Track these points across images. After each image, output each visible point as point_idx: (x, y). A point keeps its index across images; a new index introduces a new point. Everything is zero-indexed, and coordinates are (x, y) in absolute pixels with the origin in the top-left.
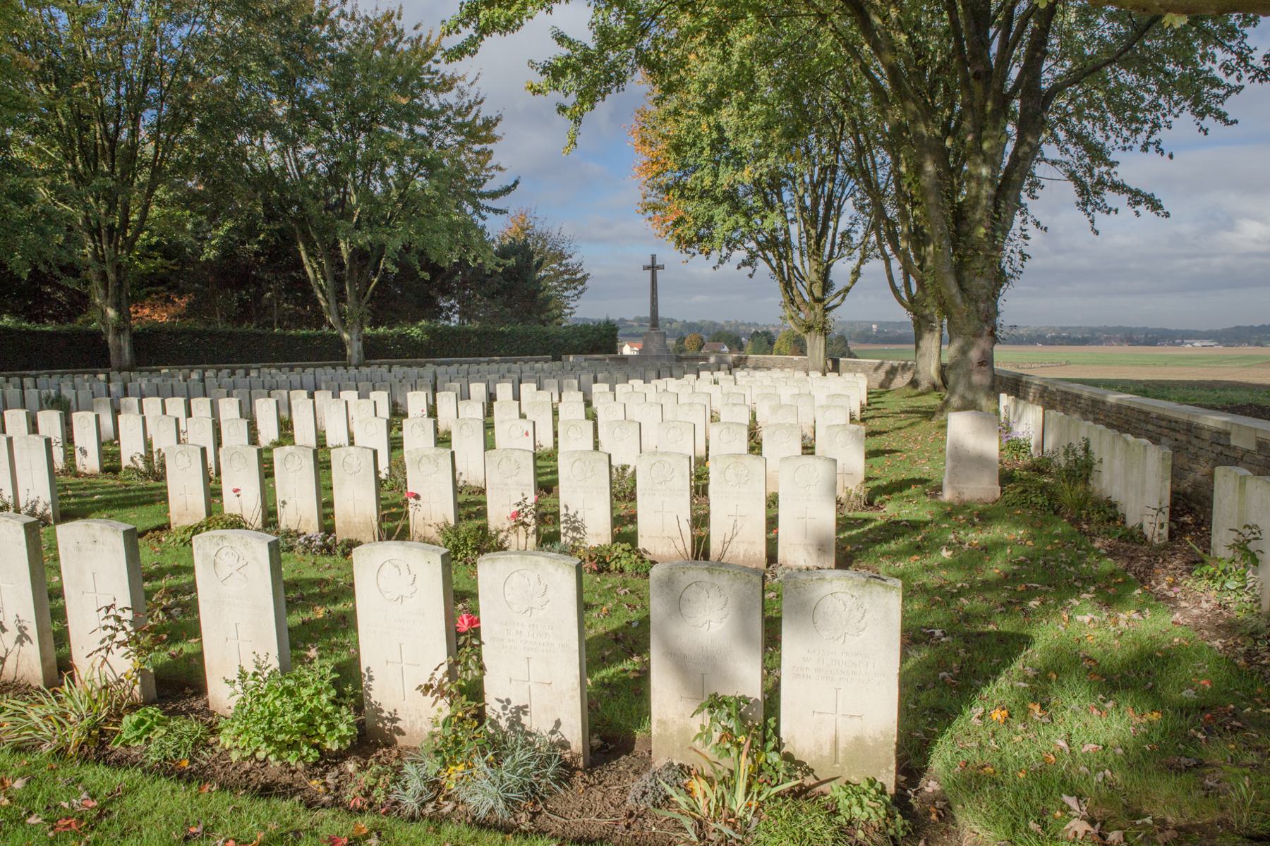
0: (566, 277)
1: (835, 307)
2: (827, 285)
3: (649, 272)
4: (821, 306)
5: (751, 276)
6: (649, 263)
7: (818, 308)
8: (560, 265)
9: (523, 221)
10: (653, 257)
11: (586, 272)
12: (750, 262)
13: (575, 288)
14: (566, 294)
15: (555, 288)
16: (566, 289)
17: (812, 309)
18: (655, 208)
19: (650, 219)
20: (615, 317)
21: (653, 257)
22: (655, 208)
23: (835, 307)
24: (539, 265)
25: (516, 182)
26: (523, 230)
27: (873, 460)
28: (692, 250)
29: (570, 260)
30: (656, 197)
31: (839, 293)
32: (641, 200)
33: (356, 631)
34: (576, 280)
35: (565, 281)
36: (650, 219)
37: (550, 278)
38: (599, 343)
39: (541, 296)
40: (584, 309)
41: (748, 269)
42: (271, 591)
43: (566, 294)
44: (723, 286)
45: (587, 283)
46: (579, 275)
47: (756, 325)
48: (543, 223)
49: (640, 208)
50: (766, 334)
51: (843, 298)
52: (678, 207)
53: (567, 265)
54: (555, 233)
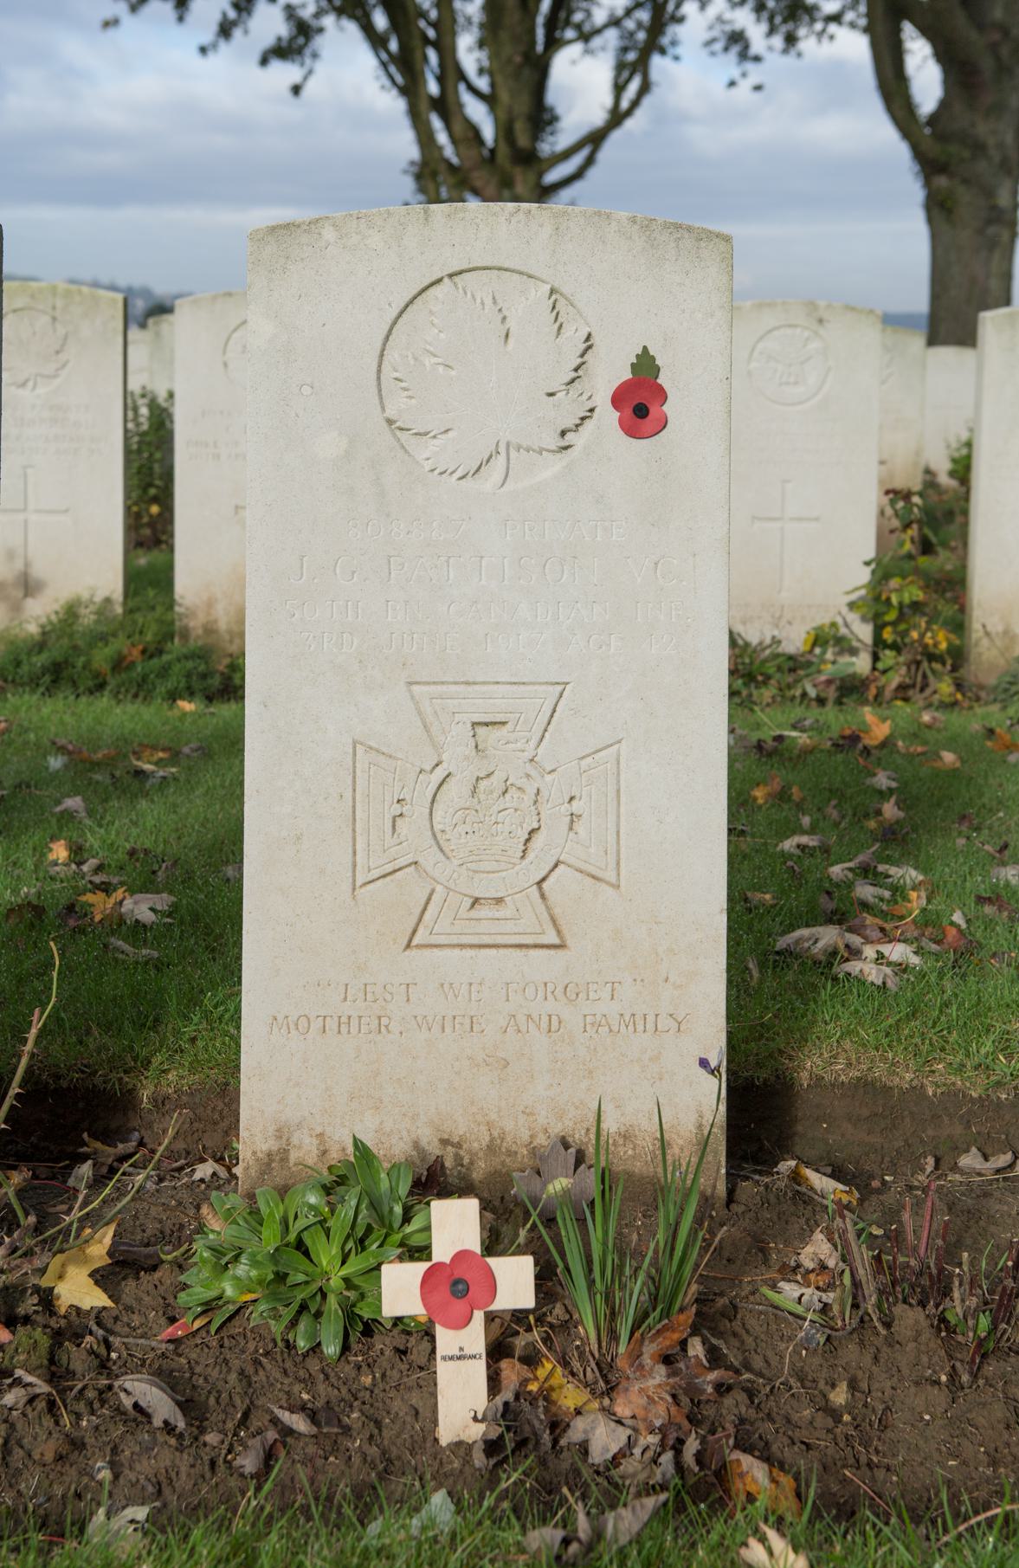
2: (541, 118)
4: (531, 177)
41: (285, 73)
51: (590, 161)
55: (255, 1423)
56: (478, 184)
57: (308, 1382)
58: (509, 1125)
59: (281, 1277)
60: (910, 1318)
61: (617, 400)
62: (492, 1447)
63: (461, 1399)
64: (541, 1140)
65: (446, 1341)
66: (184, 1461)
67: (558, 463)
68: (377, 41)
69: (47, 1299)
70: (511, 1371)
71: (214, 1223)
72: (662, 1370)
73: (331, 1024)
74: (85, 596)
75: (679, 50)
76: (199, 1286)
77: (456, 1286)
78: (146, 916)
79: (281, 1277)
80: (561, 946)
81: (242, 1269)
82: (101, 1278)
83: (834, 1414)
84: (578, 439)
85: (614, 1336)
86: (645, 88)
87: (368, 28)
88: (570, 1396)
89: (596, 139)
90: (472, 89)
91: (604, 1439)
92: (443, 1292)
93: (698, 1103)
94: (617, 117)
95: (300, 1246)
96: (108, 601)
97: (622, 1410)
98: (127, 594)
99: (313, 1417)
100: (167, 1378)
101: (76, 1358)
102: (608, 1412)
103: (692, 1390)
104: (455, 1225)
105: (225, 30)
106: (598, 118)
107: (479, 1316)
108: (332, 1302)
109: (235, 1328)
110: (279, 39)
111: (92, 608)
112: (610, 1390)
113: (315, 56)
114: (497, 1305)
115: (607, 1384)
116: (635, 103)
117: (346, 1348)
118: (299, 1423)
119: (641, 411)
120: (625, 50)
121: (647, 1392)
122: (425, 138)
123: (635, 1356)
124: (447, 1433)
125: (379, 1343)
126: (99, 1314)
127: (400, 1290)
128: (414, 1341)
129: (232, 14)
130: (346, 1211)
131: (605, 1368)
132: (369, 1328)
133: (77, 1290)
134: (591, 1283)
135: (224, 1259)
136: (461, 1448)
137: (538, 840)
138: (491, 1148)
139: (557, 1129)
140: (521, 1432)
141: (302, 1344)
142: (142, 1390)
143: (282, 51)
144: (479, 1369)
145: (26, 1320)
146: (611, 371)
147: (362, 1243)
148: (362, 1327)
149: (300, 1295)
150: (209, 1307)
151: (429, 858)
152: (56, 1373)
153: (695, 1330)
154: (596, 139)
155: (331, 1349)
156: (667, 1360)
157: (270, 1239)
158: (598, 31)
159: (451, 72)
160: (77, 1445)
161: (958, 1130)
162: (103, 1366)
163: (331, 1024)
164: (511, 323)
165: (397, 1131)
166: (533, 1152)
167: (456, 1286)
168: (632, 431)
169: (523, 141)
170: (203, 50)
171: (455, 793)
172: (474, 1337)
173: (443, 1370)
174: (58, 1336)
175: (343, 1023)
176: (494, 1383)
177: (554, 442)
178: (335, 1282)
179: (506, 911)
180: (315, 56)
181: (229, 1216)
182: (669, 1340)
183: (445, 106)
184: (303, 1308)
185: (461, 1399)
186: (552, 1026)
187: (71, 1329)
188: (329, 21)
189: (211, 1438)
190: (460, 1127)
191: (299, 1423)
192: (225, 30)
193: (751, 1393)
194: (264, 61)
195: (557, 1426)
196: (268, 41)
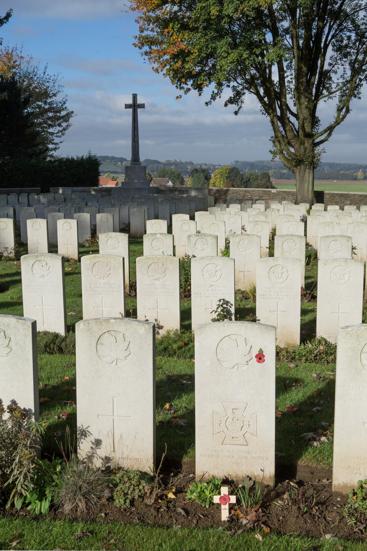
0: (51, 115)
1: (322, 142)
2: (315, 121)
3: (131, 110)
4: (310, 141)
5: (236, 113)
6: (130, 102)
7: (308, 143)
8: (45, 103)
9: (9, 60)
10: (135, 97)
11: (70, 110)
12: (236, 99)
13: (60, 125)
14: (51, 130)
15: (40, 124)
16: (50, 126)
17: (302, 143)
18: (151, 42)
19: (146, 53)
20: (98, 152)
21: (135, 97)
22: (151, 42)
23: (322, 142)
24: (27, 103)
25: (8, 16)
26: (10, 68)
27: (96, 249)
28: (185, 87)
29: (54, 99)
30: (152, 32)
31: (325, 131)
32: (138, 34)
33: (276, 418)
34: (61, 116)
35: (49, 118)
36: (146, 53)
37: (37, 116)
38: (82, 174)
39: (28, 131)
40: (67, 146)
41: (233, 107)
42: (31, 347)
43: (51, 130)
44: (224, 123)
45: (71, 120)
46: (63, 113)
47: (191, 163)
48: (28, 62)
49: (136, 41)
50: (203, 171)
51: (330, 135)
52: (184, 41)
53: (51, 104)
54: (40, 73)
55: (196, 516)
56: (293, 144)
57: (204, 511)
58: (239, 473)
59: (200, 496)
60: (295, 508)
61: (256, 357)
62: (228, 521)
63: (225, 515)
64: (244, 476)
65: (223, 507)
66: (186, 520)
67: (246, 367)
68: (261, 99)
69: (167, 496)
70: (233, 512)
71: (191, 487)
72: (255, 513)
73: (210, 456)
74: (171, 329)
75: (360, 96)
76: (189, 496)
77: (224, 499)
78: (182, 424)
79: (200, 496)
80: (247, 445)
81: (194, 494)
82: (175, 494)
83: (279, 521)
84: (250, 363)
85: (248, 507)
86: (348, 111)
87: (257, 94)
88: (241, 515)
89: (330, 129)
90: (292, 114)
91: (244, 522)
92: (222, 500)
93: (270, 469)
94: (337, 123)
95: (203, 491)
96: (177, 330)
97: (248, 518)
98: (180, 329)
99: (204, 516)
100: (184, 509)
101: (170, 505)
102: (246, 518)
103: (259, 516)
104: (225, 490)
105: (213, 98)
106: (332, 121)
107: (228, 504)
108: (208, 500)
109: (193, 502)
110: (230, 97)
111: (173, 332)
112: (247, 515)
113: (242, 102)
114: (231, 502)
115: (247, 514)
116: (344, 117)
117: (210, 506)
118: (202, 516)
119: (260, 359)
120: (342, 96)
121: (252, 516)
122: (275, 129)
123: (251, 510)
124: (223, 520)
125: (214, 506)
126: (174, 499)
127: (216, 499)
128: (218, 506)
129: (216, 91)
130: (210, 487)
131: (246, 512)
132: (213, 504)
133: (171, 496)
134: (244, 500)
135: (192, 492)
136: (224, 521)
137: (243, 428)
138: (236, 477)
139: (247, 474)
140: (234, 520)
141: (203, 506)
142: (180, 510)
143: (231, 101)
144: (228, 511)
145: (164, 499)
146: (255, 352)
147: (213, 492)
148: (212, 504)
149: (203, 498)
150: (190, 499)
151: (225, 430)
152: (168, 507)
153: (260, 507)
154: (330, 129)
155: (207, 507)
156: (256, 511)
157: (199, 490)
158: (335, 92)
159: (285, 107)
160: (171, 517)
161: (324, 475)
162: (175, 506)
163: (210, 456)
164: (238, 343)
165: (220, 473)
166: (243, 477)
167: (224, 499)
168: (258, 362)
169: (308, 130)
170: (207, 104)
171: (230, 420)
172: (227, 506)
173: (222, 511)
174: (168, 502)
175: (212, 456)
176: (230, 513)
177: (246, 363)
178: (208, 497)
179: (238, 439)
180: (242, 102)
181: (193, 486)
182: (256, 509)
183: (283, 119)
184: (203, 500)
185: (225, 515)
186: (246, 458)
187: (170, 501)
188: (246, 91)
189: (189, 518)
190: (231, 473)
191: (202, 516)
192: (213, 98)
193: (268, 517)
194: (226, 105)
195: (238, 519)
196: (227, 98)
